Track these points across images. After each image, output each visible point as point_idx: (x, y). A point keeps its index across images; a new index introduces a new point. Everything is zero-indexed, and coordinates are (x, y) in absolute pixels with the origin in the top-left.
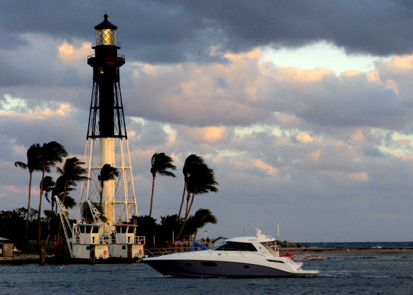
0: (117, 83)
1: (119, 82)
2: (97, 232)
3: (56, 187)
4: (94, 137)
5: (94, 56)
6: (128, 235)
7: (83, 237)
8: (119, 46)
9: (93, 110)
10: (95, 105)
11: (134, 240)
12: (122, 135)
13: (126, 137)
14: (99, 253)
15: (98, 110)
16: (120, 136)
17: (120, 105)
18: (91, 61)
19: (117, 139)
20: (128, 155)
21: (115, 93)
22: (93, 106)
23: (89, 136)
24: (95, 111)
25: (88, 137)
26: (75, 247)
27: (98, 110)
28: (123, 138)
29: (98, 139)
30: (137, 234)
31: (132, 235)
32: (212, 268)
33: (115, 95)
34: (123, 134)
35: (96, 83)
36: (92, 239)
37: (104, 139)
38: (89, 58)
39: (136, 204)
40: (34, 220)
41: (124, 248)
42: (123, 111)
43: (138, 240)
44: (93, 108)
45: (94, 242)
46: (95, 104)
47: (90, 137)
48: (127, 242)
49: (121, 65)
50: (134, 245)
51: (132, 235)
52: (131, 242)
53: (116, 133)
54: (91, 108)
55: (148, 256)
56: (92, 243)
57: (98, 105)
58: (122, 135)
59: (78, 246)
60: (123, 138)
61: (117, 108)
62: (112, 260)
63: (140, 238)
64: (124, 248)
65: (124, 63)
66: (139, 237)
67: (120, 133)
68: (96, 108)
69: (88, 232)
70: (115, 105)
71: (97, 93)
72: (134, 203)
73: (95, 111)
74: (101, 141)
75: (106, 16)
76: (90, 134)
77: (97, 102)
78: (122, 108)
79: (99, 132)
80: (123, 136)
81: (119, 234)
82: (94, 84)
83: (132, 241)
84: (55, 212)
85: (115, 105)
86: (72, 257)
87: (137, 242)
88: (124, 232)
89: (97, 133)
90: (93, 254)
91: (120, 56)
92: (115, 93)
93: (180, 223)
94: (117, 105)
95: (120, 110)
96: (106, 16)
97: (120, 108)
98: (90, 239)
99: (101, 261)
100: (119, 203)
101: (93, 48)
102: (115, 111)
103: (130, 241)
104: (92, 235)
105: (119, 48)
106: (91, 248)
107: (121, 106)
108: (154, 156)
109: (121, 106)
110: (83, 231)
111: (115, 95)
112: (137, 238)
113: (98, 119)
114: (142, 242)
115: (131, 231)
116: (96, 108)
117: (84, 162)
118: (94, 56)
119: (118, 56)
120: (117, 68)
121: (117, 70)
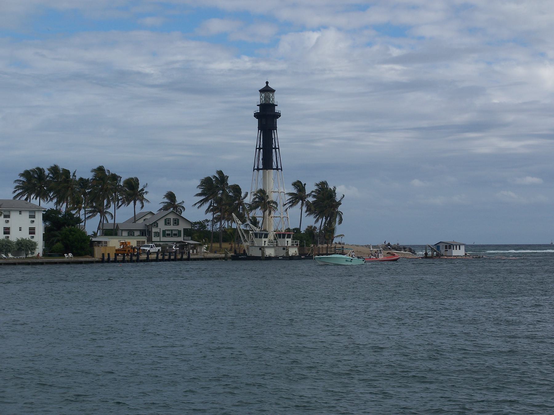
4: (258, 169)
7: (257, 241)
9: (258, 150)
14: (270, 252)
16: (277, 169)
17: (277, 147)
22: (258, 147)
24: (259, 150)
26: (251, 249)
29: (261, 171)
30: (294, 238)
31: (290, 240)
32: (111, 256)
34: (279, 167)
36: (263, 242)
41: (284, 249)
51: (290, 240)
53: (275, 167)
55: (456, 252)
57: (261, 147)
61: (275, 148)
62: (276, 258)
63: (296, 242)
67: (277, 167)
68: (260, 149)
69: (261, 237)
73: (259, 150)
75: (267, 83)
76: (256, 167)
88: (284, 237)
89: (261, 166)
94: (275, 146)
95: (277, 150)
96: (267, 83)
102: (274, 150)
104: (264, 240)
108: (38, 169)
110: (280, 237)
113: (261, 157)
115: (289, 237)
116: (260, 149)
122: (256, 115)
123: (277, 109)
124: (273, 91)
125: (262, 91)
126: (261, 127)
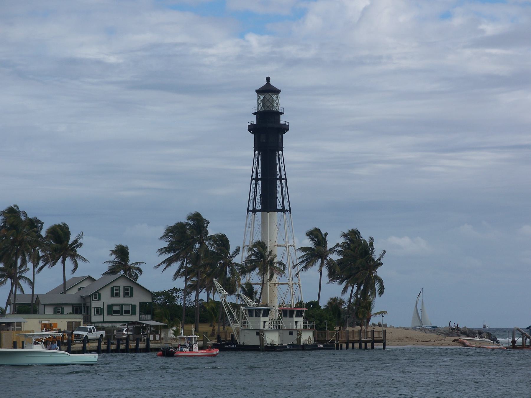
0: (280, 152)
2: (267, 315)
3: (217, 262)
4: (254, 211)
5: (255, 123)
6: (295, 319)
9: (254, 181)
13: (290, 211)
15: (260, 182)
16: (283, 210)
17: (283, 177)
18: (252, 129)
21: (278, 163)
22: (254, 177)
26: (242, 333)
27: (260, 182)
29: (259, 214)
30: (306, 319)
34: (287, 208)
35: (257, 152)
36: (262, 323)
38: (250, 124)
40: (213, 301)
44: (254, 179)
45: (264, 327)
47: (251, 211)
48: (295, 328)
49: (285, 133)
50: (302, 330)
52: (298, 328)
53: (280, 207)
54: (252, 179)
57: (259, 177)
59: (246, 331)
61: (281, 179)
62: (282, 348)
63: (309, 323)
64: (291, 334)
65: (288, 130)
67: (284, 207)
68: (257, 180)
70: (278, 177)
71: (258, 163)
72: (299, 284)
75: (268, 79)
76: (251, 208)
78: (286, 179)
80: (287, 211)
82: (290, 207)
84: (325, 278)
85: (278, 177)
89: (259, 207)
90: (262, 340)
91: (284, 123)
92: (278, 163)
95: (284, 181)
96: (268, 79)
97: (283, 179)
99: (272, 348)
102: (278, 182)
104: (263, 319)
105: (283, 113)
106: (259, 333)
110: (285, 315)
114: (312, 327)
115: (299, 314)
116: (257, 180)
117: (249, 106)
118: (255, 123)
120: (280, 136)
121: (280, 137)
122: (252, 129)
123: (283, 120)
124: (277, 92)
125: (259, 92)
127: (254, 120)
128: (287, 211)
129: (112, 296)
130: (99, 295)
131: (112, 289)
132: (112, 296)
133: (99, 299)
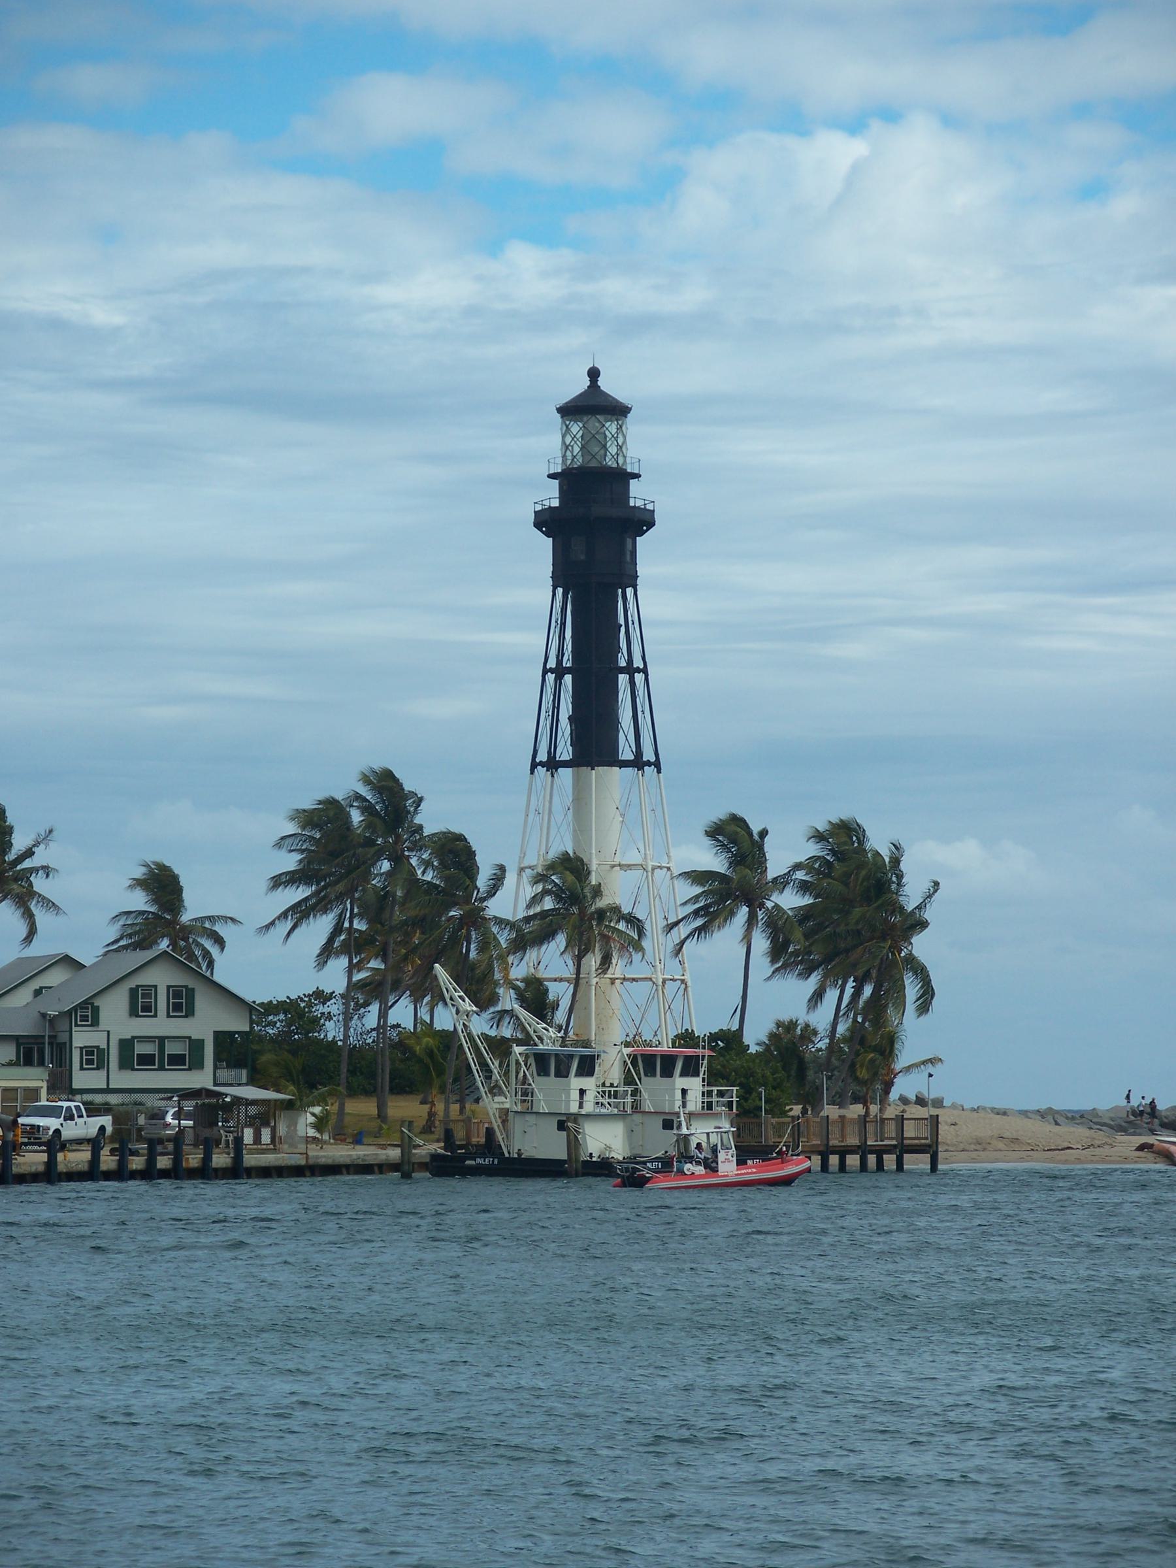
0: (629, 591)
1: (635, 587)
2: (591, 1073)
4: (553, 764)
5: (555, 503)
6: (680, 1082)
8: (636, 471)
9: (551, 677)
10: (559, 661)
11: (700, 1099)
12: (645, 759)
13: (657, 765)
15: (568, 679)
16: (638, 763)
17: (638, 663)
18: (545, 521)
19: (630, 771)
20: (1092, 1162)
21: (622, 621)
22: (552, 664)
23: (538, 760)
25: (534, 765)
26: (517, 1125)
27: (568, 679)
28: (646, 768)
29: (566, 774)
31: (695, 1085)
33: (623, 629)
34: (648, 755)
35: (560, 591)
36: (575, 1095)
37: (585, 770)
38: (539, 508)
39: (689, 984)
42: (647, 679)
43: (714, 1099)
44: (552, 671)
45: (581, 1106)
46: (558, 657)
47: (542, 764)
49: (642, 533)
51: (695, 1085)
53: (627, 754)
54: (545, 671)
56: (574, 1108)
57: (567, 663)
58: (645, 759)
60: (646, 768)
61: (630, 670)
66: (715, 1089)
67: (639, 753)
68: (560, 672)
70: (622, 663)
71: (563, 624)
72: (683, 981)
74: (577, 781)
75: (594, 374)
76: (542, 756)
77: (563, 655)
78: (645, 671)
79: (570, 749)
80: (649, 764)
81: (650, 1080)
82: (544, 680)
83: (695, 1101)
86: (507, 1155)
87: (710, 1106)
89: (565, 752)
90: (574, 1144)
91: (639, 503)
92: (622, 621)
93: (386, 866)
95: (639, 678)
96: (594, 374)
97: (638, 670)
98: (568, 1095)
99: (602, 1168)
100: (634, 980)
101: (551, 476)
102: (623, 679)
103: (688, 1104)
104: (576, 1083)
107: (641, 667)
109: (641, 667)
111: (623, 629)
112: (710, 1093)
113: (566, 709)
115: (691, 1068)
116: (560, 672)
118: (555, 503)
119: (632, 504)
120: (629, 541)
122: (545, 521)
125: (569, 411)
126: (565, 574)
127: (551, 495)
128: (649, 764)
129: (134, 1013)
130: (96, 1011)
131: (133, 992)
132: (134, 1013)
133: (95, 1022)
